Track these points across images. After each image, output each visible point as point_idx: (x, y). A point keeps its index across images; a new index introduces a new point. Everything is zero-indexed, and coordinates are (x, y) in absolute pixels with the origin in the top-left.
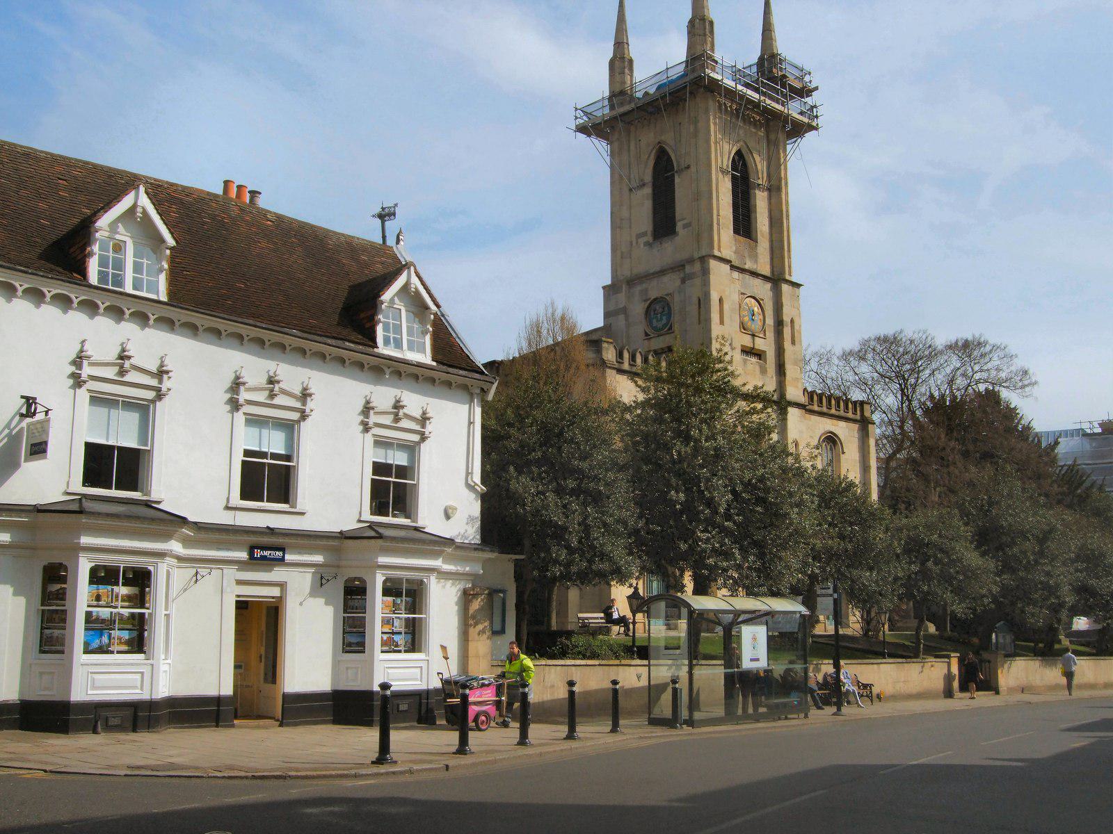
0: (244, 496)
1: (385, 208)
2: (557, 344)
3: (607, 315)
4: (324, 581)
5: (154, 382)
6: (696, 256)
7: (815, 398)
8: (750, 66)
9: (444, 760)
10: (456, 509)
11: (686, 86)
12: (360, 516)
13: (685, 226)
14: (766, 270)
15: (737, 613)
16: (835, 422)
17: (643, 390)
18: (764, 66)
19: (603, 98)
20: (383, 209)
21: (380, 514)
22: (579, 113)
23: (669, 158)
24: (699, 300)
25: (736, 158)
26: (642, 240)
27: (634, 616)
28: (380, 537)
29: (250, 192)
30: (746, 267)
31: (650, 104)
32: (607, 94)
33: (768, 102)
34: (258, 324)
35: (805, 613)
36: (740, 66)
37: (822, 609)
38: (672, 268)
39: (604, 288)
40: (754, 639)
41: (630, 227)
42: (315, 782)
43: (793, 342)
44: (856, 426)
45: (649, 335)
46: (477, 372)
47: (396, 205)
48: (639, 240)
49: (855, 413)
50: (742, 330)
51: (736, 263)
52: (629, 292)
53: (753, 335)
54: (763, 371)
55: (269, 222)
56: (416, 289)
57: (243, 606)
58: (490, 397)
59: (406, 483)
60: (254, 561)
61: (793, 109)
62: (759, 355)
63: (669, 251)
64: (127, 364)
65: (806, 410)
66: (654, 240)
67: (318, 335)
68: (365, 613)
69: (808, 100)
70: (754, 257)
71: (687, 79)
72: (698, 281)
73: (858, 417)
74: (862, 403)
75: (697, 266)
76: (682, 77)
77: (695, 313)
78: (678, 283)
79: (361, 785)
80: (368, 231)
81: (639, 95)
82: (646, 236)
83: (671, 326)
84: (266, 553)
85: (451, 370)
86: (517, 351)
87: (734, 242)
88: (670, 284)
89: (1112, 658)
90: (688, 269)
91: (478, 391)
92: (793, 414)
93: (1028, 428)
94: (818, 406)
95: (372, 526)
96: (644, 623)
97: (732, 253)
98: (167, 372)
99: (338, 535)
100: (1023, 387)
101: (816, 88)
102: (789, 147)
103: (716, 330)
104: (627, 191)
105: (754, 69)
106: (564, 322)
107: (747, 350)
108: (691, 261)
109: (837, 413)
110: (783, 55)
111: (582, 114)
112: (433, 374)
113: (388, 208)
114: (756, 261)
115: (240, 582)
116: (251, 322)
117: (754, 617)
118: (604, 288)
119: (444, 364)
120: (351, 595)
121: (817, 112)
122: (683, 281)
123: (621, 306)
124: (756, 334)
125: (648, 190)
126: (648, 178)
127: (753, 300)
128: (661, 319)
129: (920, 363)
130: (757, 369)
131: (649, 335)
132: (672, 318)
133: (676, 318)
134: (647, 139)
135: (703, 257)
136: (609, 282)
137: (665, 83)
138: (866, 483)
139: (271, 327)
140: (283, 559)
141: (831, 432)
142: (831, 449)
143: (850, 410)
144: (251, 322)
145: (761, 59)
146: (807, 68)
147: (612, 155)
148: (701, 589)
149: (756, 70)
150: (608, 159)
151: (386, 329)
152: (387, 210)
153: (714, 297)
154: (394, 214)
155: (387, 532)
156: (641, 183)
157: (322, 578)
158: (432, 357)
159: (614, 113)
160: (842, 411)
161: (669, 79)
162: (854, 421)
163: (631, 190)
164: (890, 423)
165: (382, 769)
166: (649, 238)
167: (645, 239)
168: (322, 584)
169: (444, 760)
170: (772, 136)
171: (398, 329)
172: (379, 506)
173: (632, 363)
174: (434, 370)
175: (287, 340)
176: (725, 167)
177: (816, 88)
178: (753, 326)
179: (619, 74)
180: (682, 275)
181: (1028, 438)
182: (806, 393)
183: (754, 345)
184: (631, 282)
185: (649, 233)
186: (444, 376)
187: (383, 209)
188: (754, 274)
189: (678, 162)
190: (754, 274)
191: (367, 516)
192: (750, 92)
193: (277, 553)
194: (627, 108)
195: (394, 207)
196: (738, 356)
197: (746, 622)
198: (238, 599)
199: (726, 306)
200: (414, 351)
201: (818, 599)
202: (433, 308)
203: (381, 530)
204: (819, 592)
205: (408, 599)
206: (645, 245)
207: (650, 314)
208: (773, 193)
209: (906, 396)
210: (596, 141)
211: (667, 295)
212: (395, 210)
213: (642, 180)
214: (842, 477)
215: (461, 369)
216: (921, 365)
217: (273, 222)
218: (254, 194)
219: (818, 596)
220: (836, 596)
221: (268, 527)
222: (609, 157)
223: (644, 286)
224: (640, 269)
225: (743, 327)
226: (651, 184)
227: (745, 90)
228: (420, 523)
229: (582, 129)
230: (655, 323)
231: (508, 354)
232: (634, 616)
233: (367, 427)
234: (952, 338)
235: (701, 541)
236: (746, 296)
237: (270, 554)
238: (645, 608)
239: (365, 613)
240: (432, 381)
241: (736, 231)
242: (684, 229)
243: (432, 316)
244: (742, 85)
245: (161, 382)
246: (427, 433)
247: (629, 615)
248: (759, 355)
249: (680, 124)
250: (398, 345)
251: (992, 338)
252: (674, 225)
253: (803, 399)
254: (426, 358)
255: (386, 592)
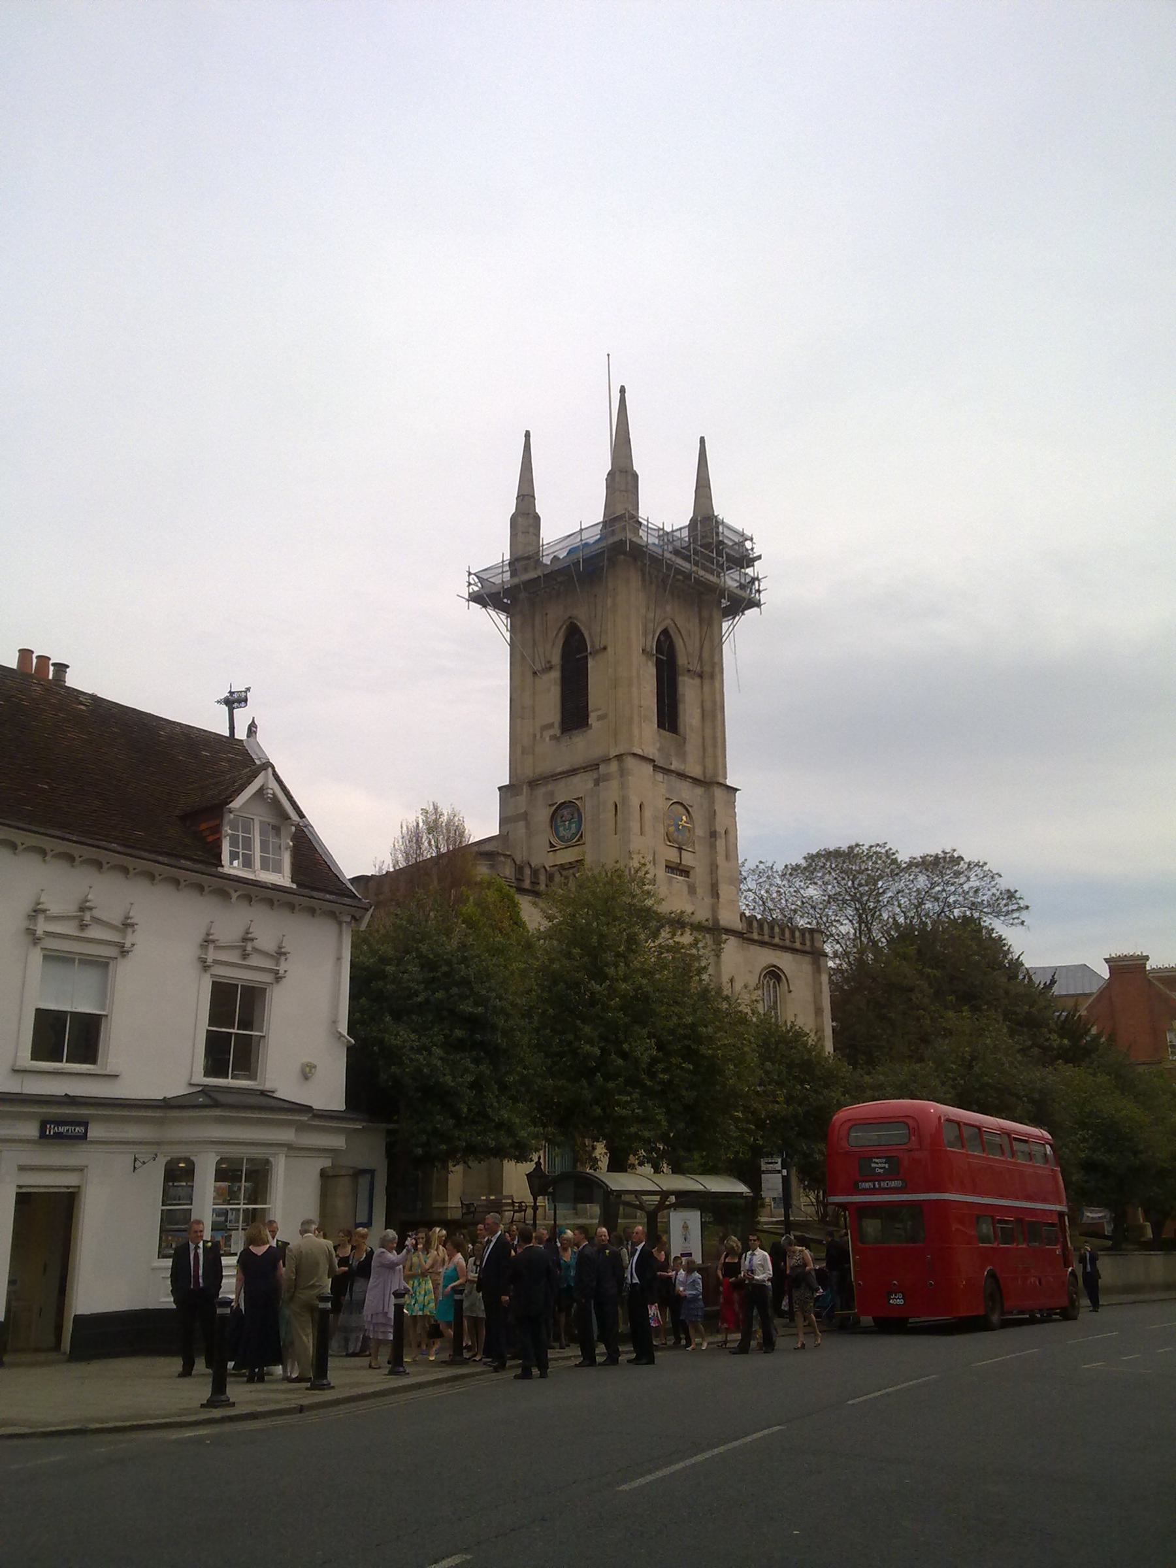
0: (35, 1057)
1: (234, 693)
2: (440, 856)
3: (503, 821)
4: (138, 1164)
5: (268, 964)
6: (613, 753)
7: (755, 924)
8: (681, 529)
9: (296, 1399)
10: (315, 1067)
11: (604, 551)
12: (191, 1078)
13: (600, 718)
14: (695, 771)
15: (665, 1194)
16: (779, 953)
17: (550, 918)
18: (697, 530)
19: (503, 561)
20: (231, 693)
21: (216, 1075)
22: (473, 579)
23: (582, 635)
24: (616, 806)
25: (662, 638)
26: (547, 734)
27: (535, 1200)
28: (216, 1105)
29: (54, 665)
30: (673, 767)
31: (559, 572)
32: (507, 557)
33: (702, 573)
34: (68, 836)
35: (747, 1194)
36: (668, 529)
37: (768, 1189)
38: (584, 768)
39: (500, 788)
40: (685, 1227)
41: (534, 719)
42: (134, 1435)
43: (727, 858)
44: (807, 959)
45: (555, 847)
46: (348, 896)
47: (248, 689)
48: (544, 733)
49: (761, 933)
50: (669, 844)
51: (660, 762)
52: (531, 795)
53: (680, 849)
54: (692, 890)
55: (82, 707)
56: (274, 794)
57: (24, 1200)
58: (363, 926)
59: (251, 1035)
60: (46, 1138)
61: (731, 580)
62: (685, 872)
63: (580, 747)
64: (87, 917)
65: (744, 939)
66: (562, 733)
67: (145, 850)
68: (191, 1204)
69: (749, 571)
70: (682, 756)
71: (603, 544)
72: (614, 784)
73: (808, 947)
74: (812, 931)
75: (614, 766)
76: (597, 541)
77: (611, 824)
78: (591, 784)
79: (189, 1436)
80: (214, 722)
81: (547, 560)
82: (554, 727)
83: (581, 836)
84: (62, 1129)
85: (315, 894)
86: (391, 865)
87: (687, 737)
88: (580, 786)
89: (1175, 1252)
90: (603, 768)
91: (348, 919)
92: (731, 946)
93: (1017, 964)
94: (759, 934)
95: (206, 1090)
96: (545, 1206)
97: (656, 752)
98: (285, 954)
99: (162, 1104)
100: (1007, 913)
101: (759, 557)
102: (725, 625)
103: (637, 843)
104: (531, 674)
105: (685, 533)
106: (455, 831)
107: (673, 865)
108: (607, 760)
109: (781, 943)
110: (720, 517)
111: (477, 580)
112: (291, 898)
113: (238, 692)
114: (684, 761)
115: (22, 1168)
116: (58, 833)
117: (686, 1200)
118: (500, 788)
119: (306, 887)
120: (174, 1181)
121: (759, 585)
122: (597, 782)
123: (522, 811)
124: (684, 847)
125: (556, 675)
126: (556, 659)
127: (680, 808)
128: (570, 828)
129: (880, 883)
130: (685, 889)
131: (555, 847)
132: (583, 826)
133: (587, 827)
134: (555, 615)
135: (621, 755)
136: (506, 781)
137: (578, 546)
138: (819, 1030)
139: (83, 839)
140: (84, 1137)
141: (775, 966)
142: (775, 987)
143: (755, 931)
144: (58, 833)
145: (693, 522)
146: (748, 533)
147: (513, 630)
148: (618, 1165)
149: (687, 534)
150: (508, 635)
151: (234, 842)
152: (235, 696)
153: (635, 802)
154: (246, 700)
155: (221, 1098)
156: (548, 666)
157: (135, 1160)
158: (292, 878)
159: (516, 580)
160: (788, 941)
161: (583, 542)
162: (804, 952)
163: (535, 673)
164: (846, 954)
165: (217, 1413)
166: (557, 731)
167: (552, 732)
168: (135, 1167)
169: (296, 1399)
170: (705, 614)
171: (248, 843)
172: (216, 1061)
173: (518, 876)
174: (295, 894)
175: (102, 855)
176: (648, 649)
177: (759, 557)
178: (680, 837)
179: (523, 533)
180: (595, 776)
181: (1017, 977)
182: (744, 918)
183: (681, 861)
184: (533, 784)
185: (557, 725)
186: (306, 902)
187: (231, 693)
188: (682, 776)
189: (592, 642)
190: (682, 776)
191: (200, 1078)
192: (679, 561)
193: (77, 1129)
194: (532, 575)
195: (246, 692)
196: (661, 873)
197: (675, 1206)
198: (21, 1191)
199: (648, 813)
200: (268, 870)
201: (763, 1175)
202: (294, 816)
203: (214, 1095)
204: (764, 1167)
205: (248, 1184)
206: (550, 740)
207: (556, 821)
208: (707, 682)
209: (864, 918)
210: (493, 613)
211: (577, 799)
212: (246, 696)
213: (549, 662)
214: (789, 1024)
215: (331, 893)
216: (881, 887)
217: (86, 706)
218: (61, 668)
219: (764, 1172)
220: (785, 1172)
221: (66, 1094)
222: (508, 634)
223: (550, 787)
224: (545, 767)
225: (669, 838)
226: (559, 667)
227: (674, 558)
228: (268, 1086)
229: (475, 598)
230: (562, 832)
231: (380, 868)
232: (535, 1200)
233: (206, 964)
234: (918, 854)
235: (618, 1105)
236: (672, 802)
237: (68, 1131)
238: (551, 1190)
239: (191, 1204)
240: (292, 907)
241: (661, 725)
242: (598, 720)
243: (293, 829)
244: (671, 552)
245: (277, 964)
246: (282, 972)
247: (529, 1199)
248: (685, 872)
249: (596, 596)
250: (248, 863)
251: (969, 854)
252: (587, 717)
253: (739, 926)
254: (283, 878)
255: (220, 1175)
